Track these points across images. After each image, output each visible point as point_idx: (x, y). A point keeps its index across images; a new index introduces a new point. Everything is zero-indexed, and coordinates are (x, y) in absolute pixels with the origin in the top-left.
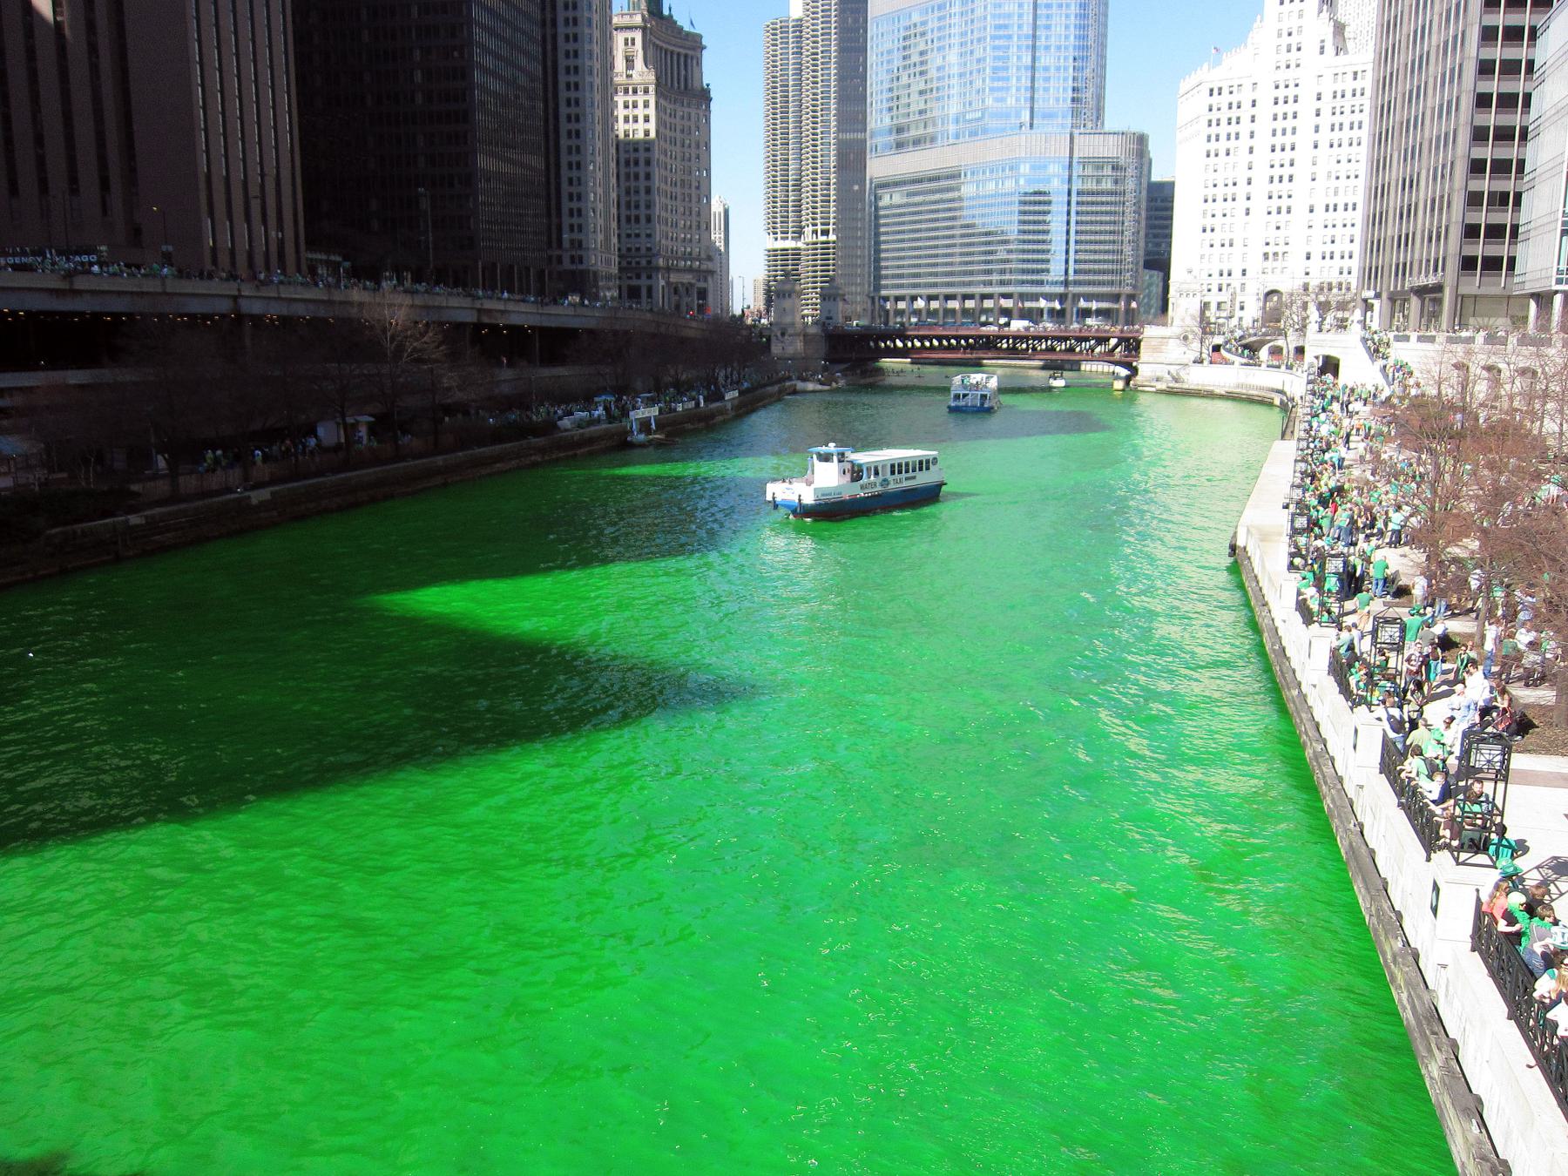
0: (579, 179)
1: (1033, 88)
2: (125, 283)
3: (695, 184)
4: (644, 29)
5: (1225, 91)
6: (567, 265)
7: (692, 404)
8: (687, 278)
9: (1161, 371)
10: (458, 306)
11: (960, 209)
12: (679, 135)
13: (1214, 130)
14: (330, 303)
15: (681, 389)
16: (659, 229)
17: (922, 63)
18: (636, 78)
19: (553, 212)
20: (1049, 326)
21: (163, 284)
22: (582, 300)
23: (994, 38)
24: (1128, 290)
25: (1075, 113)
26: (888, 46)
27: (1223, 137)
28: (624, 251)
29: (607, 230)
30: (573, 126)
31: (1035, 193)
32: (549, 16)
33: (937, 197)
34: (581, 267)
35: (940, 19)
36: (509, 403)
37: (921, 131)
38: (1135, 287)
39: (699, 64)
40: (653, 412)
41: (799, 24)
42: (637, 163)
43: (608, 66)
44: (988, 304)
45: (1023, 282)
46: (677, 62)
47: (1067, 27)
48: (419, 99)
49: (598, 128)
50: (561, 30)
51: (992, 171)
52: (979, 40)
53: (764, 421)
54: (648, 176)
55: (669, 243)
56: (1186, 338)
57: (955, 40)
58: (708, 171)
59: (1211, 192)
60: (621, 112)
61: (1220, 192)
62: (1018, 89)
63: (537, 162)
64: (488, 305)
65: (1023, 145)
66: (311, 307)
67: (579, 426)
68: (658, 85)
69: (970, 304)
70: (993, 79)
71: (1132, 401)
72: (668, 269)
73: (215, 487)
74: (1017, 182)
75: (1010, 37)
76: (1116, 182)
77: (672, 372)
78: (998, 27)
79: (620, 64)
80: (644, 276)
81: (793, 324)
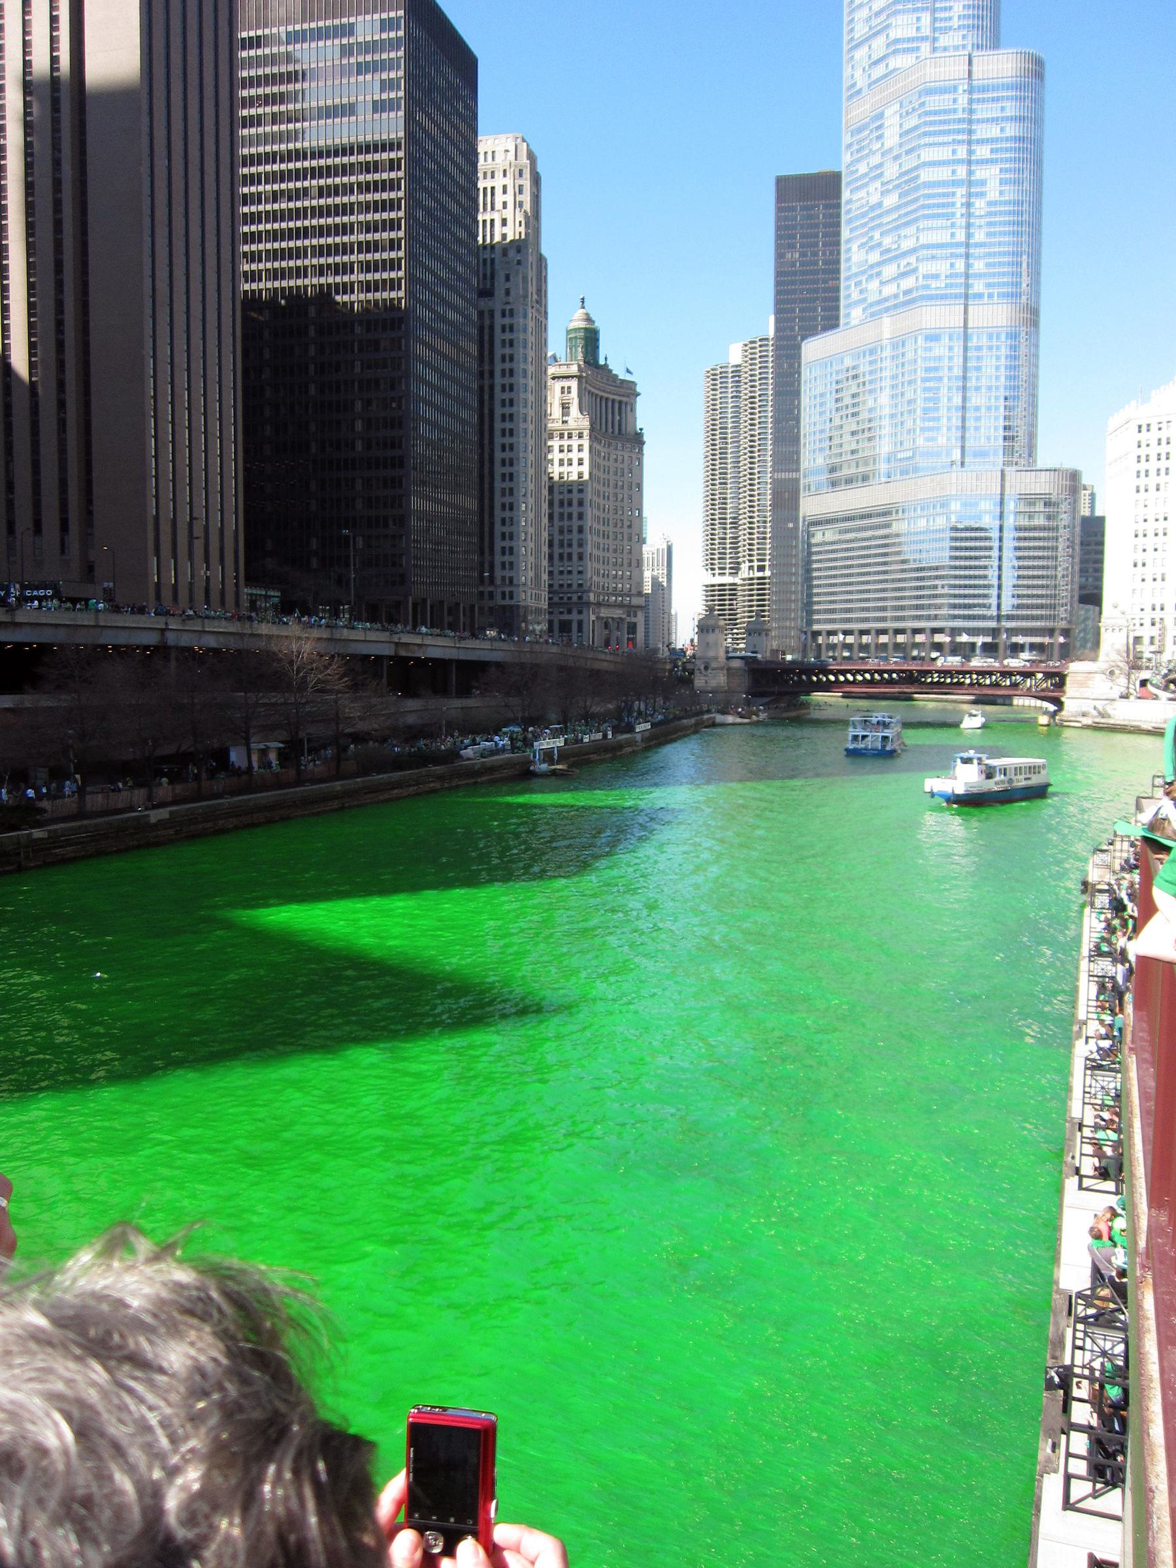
0: (511, 519)
1: (963, 427)
2: (66, 618)
3: (626, 523)
4: (579, 378)
5: (1154, 428)
6: (499, 601)
7: (599, 736)
8: (618, 613)
9: (1087, 706)
10: (371, 639)
11: (900, 544)
12: (612, 477)
13: (1143, 466)
14: (241, 635)
15: (589, 719)
16: (590, 566)
17: (854, 405)
18: (572, 424)
19: (487, 550)
20: (977, 663)
21: (97, 619)
22: (499, 633)
23: (924, 380)
24: (1063, 624)
25: (1009, 451)
26: (820, 390)
27: (1153, 473)
28: (556, 587)
29: (537, 567)
30: (507, 470)
31: (967, 529)
32: (487, 368)
33: (869, 534)
34: (512, 602)
35: (871, 363)
36: (413, 734)
37: (853, 470)
38: (1070, 622)
39: (633, 410)
40: (560, 742)
41: (737, 371)
42: (570, 504)
43: (542, 415)
44: (920, 638)
45: (955, 617)
46: (611, 408)
47: (997, 368)
48: (359, 446)
49: (531, 472)
50: (498, 380)
51: (922, 509)
52: (910, 382)
53: (681, 754)
54: (581, 516)
55: (601, 580)
56: (1112, 673)
57: (887, 383)
58: (640, 510)
59: (1141, 527)
60: (556, 456)
61: (1151, 527)
62: (949, 429)
63: (472, 504)
64: (406, 639)
65: (956, 482)
66: (221, 639)
67: (482, 756)
68: (592, 430)
69: (901, 639)
70: (924, 420)
71: (1058, 735)
72: (599, 604)
73: (120, 806)
74: (948, 519)
75: (940, 379)
76: (1049, 518)
77: (581, 704)
78: (928, 370)
79: (556, 411)
80: (575, 612)
81: (716, 658)
